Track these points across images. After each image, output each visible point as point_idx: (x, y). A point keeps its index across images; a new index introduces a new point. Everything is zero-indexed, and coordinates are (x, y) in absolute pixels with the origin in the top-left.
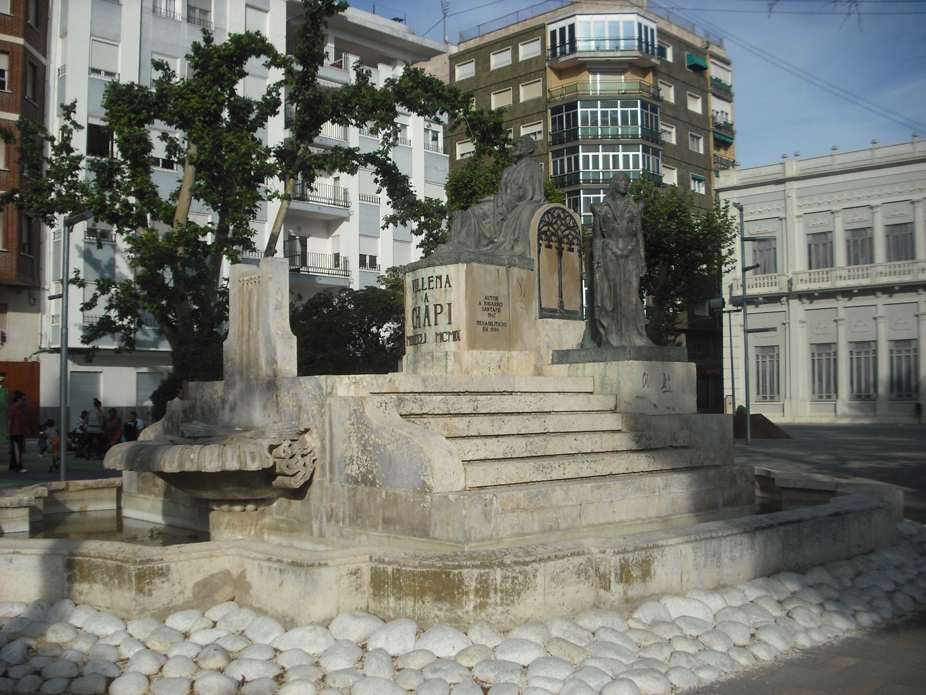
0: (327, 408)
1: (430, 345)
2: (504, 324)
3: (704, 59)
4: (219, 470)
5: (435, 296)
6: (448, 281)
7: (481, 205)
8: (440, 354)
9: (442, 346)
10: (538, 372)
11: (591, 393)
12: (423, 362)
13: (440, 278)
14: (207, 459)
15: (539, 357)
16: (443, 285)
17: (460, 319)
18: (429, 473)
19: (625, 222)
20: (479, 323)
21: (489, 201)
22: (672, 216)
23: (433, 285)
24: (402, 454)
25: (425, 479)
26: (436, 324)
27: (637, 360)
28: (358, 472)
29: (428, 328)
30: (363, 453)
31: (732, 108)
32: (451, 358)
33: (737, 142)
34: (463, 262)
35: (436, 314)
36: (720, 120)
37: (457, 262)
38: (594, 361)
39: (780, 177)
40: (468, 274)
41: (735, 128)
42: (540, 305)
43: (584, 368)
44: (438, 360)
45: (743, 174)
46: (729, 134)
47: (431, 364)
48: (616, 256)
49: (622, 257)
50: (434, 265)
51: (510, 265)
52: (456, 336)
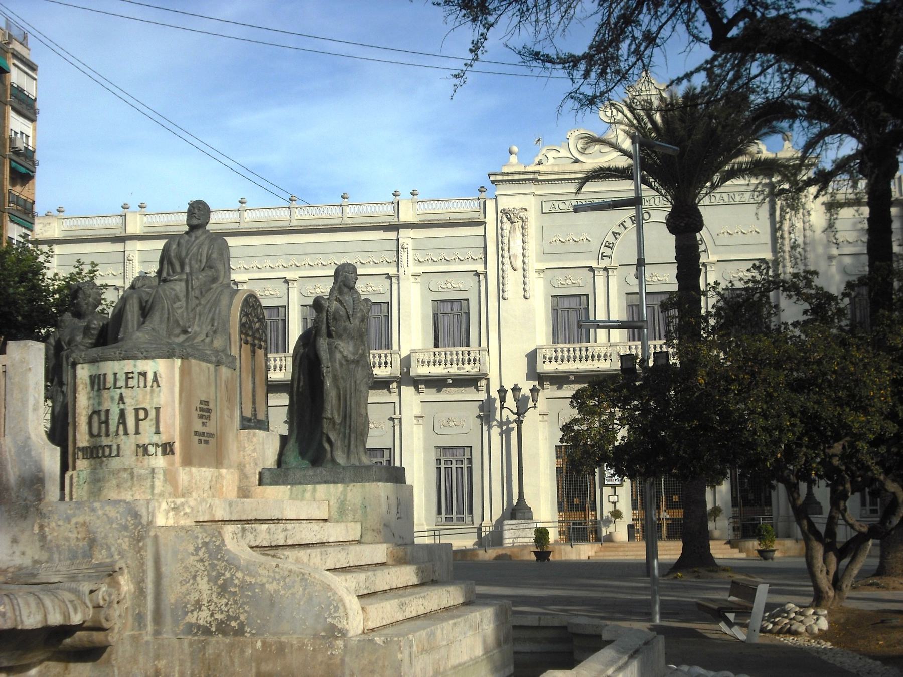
0: (149, 541)
1: (128, 458)
2: (211, 435)
3: (5, 58)
4: (39, 626)
5: (134, 398)
6: (155, 379)
7: (171, 285)
8: (143, 472)
9: (146, 462)
10: (244, 493)
11: (325, 520)
12: (114, 482)
13: (144, 374)
14: (25, 613)
15: (243, 476)
16: (149, 384)
17: (172, 425)
18: (342, 614)
19: (357, 322)
20: (196, 433)
21: (181, 280)
22: (23, 278)
23: (131, 383)
24: (293, 594)
25: (335, 622)
26: (137, 433)
27: (387, 481)
28: (209, 619)
29: (123, 437)
30: (220, 595)
31: (35, 130)
32: (160, 477)
33: (40, 174)
34: (179, 357)
35: (138, 420)
36: (20, 145)
37: (170, 355)
38: (325, 483)
39: (118, 233)
40: (183, 372)
41: (37, 157)
42: (242, 412)
43: (314, 491)
44: (141, 478)
45: (67, 224)
46: (28, 165)
47: (129, 484)
48: (347, 360)
49: (353, 361)
50: (135, 358)
51: (218, 363)
52: (167, 449)
